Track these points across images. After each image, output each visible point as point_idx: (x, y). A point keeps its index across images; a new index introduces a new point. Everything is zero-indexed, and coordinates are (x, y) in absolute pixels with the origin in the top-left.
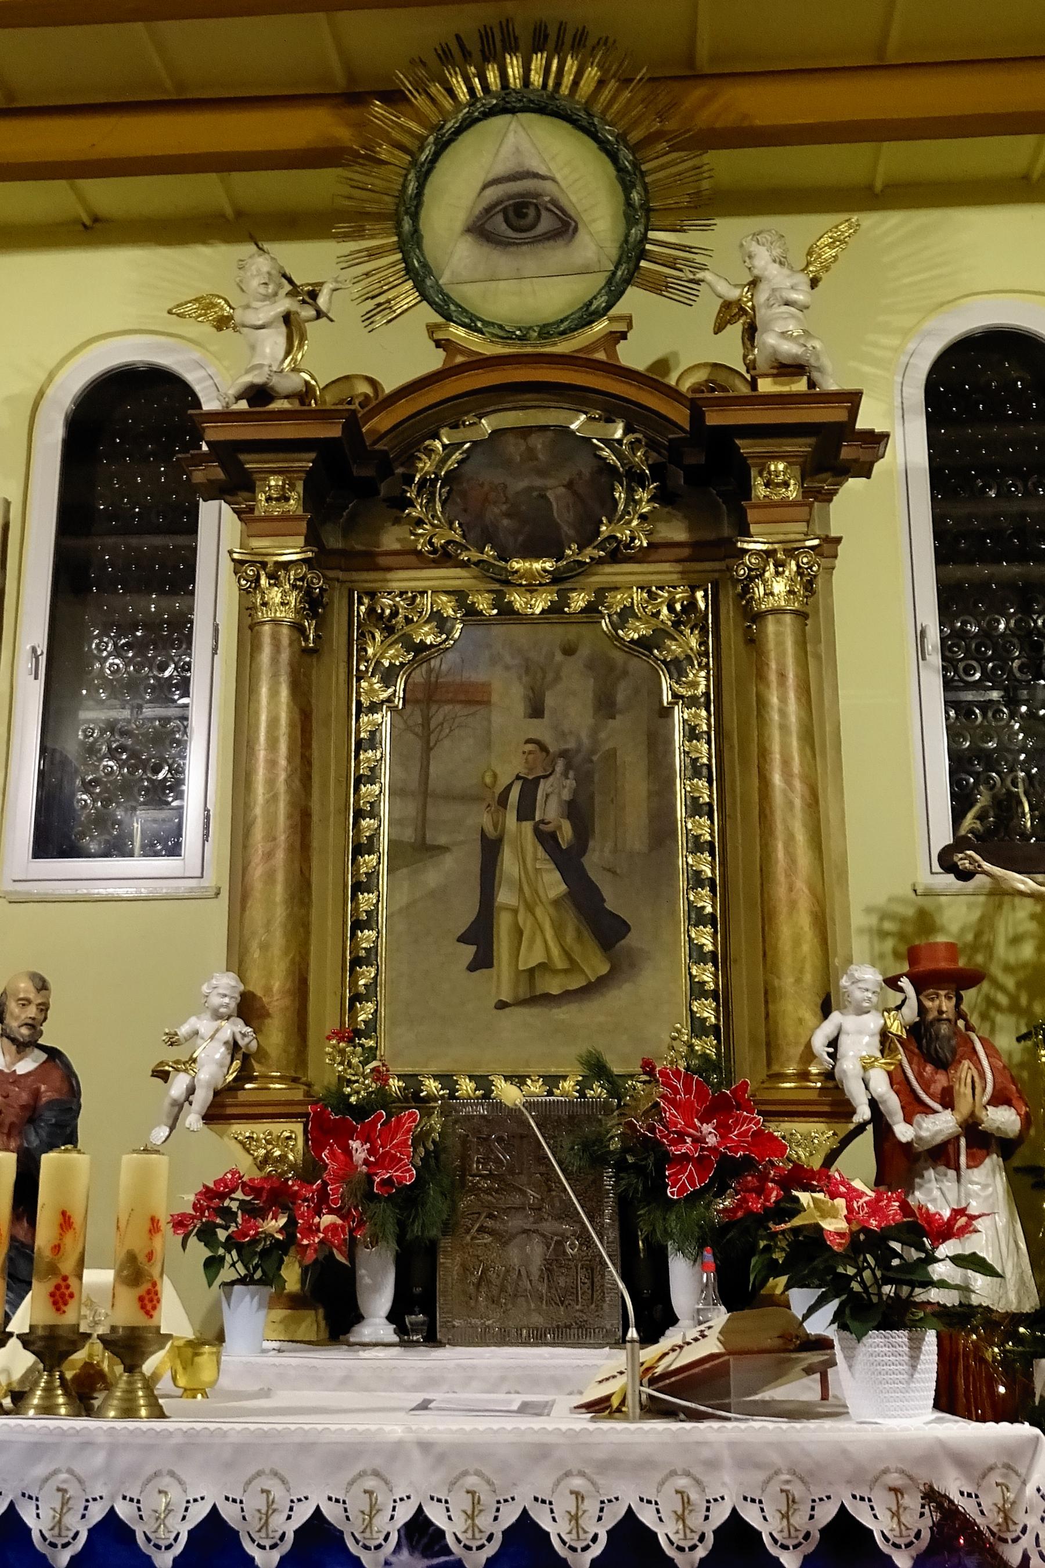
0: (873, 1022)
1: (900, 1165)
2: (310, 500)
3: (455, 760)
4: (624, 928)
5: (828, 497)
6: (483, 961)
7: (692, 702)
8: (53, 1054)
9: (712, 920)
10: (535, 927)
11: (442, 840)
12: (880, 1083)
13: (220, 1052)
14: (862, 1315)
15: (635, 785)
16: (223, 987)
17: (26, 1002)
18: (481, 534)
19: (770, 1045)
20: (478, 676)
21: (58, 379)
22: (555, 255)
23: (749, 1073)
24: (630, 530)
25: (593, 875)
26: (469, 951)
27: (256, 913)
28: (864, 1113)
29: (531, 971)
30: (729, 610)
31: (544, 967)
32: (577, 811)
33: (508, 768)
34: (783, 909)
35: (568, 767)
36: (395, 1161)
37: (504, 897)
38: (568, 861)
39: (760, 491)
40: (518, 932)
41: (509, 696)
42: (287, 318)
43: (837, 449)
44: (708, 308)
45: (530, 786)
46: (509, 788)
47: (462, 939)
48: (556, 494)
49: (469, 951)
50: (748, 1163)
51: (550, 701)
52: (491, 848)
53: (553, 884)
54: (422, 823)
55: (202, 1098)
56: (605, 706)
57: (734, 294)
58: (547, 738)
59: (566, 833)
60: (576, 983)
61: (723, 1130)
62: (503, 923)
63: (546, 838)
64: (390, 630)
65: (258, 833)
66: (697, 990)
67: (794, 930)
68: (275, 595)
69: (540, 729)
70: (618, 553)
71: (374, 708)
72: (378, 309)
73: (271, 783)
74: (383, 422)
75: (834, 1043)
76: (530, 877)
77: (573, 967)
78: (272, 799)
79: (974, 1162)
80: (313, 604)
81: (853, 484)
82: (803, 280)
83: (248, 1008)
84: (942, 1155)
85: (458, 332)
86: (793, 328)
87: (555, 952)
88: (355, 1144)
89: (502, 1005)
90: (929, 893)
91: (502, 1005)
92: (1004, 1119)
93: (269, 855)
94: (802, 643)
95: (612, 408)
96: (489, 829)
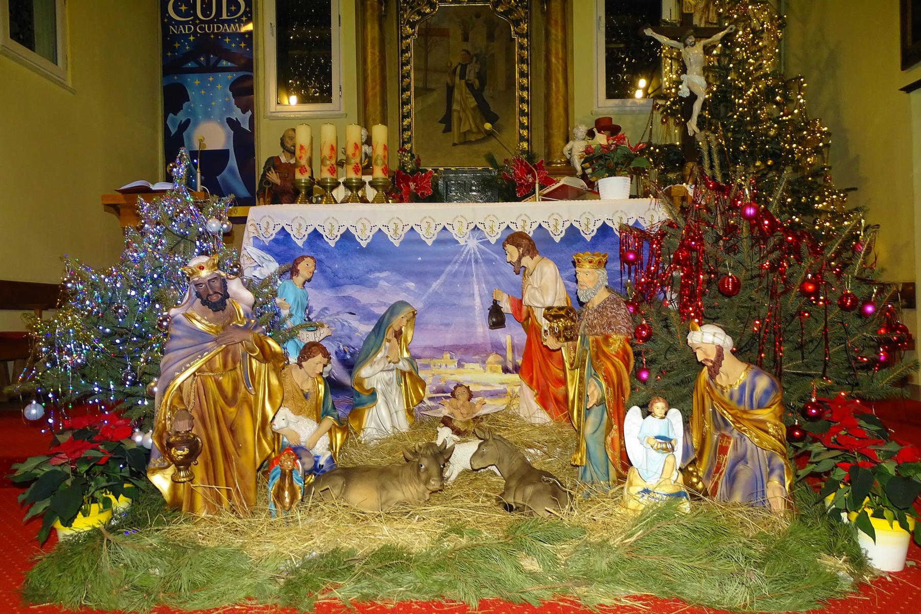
4: (498, 118)
6: (448, 129)
9: (527, 114)
10: (466, 122)
11: (433, 87)
15: (501, 66)
25: (486, 99)
27: (370, 108)
29: (465, 133)
31: (469, 131)
32: (481, 76)
33: (456, 60)
34: (554, 106)
35: (477, 60)
36: (425, 188)
37: (455, 107)
38: (478, 94)
40: (460, 119)
41: (456, 33)
45: (464, 67)
46: (456, 68)
47: (440, 122)
51: (471, 36)
52: (450, 90)
53: (472, 102)
54: (425, 80)
56: (491, 37)
58: (470, 49)
59: (477, 84)
60: (480, 137)
62: (455, 116)
63: (470, 86)
65: (370, 79)
67: (557, 112)
69: (468, 46)
73: (373, 61)
75: (571, 150)
76: (464, 100)
78: (374, 68)
87: (473, 126)
88: (411, 183)
89: (455, 145)
91: (455, 145)
93: (374, 88)
96: (450, 82)
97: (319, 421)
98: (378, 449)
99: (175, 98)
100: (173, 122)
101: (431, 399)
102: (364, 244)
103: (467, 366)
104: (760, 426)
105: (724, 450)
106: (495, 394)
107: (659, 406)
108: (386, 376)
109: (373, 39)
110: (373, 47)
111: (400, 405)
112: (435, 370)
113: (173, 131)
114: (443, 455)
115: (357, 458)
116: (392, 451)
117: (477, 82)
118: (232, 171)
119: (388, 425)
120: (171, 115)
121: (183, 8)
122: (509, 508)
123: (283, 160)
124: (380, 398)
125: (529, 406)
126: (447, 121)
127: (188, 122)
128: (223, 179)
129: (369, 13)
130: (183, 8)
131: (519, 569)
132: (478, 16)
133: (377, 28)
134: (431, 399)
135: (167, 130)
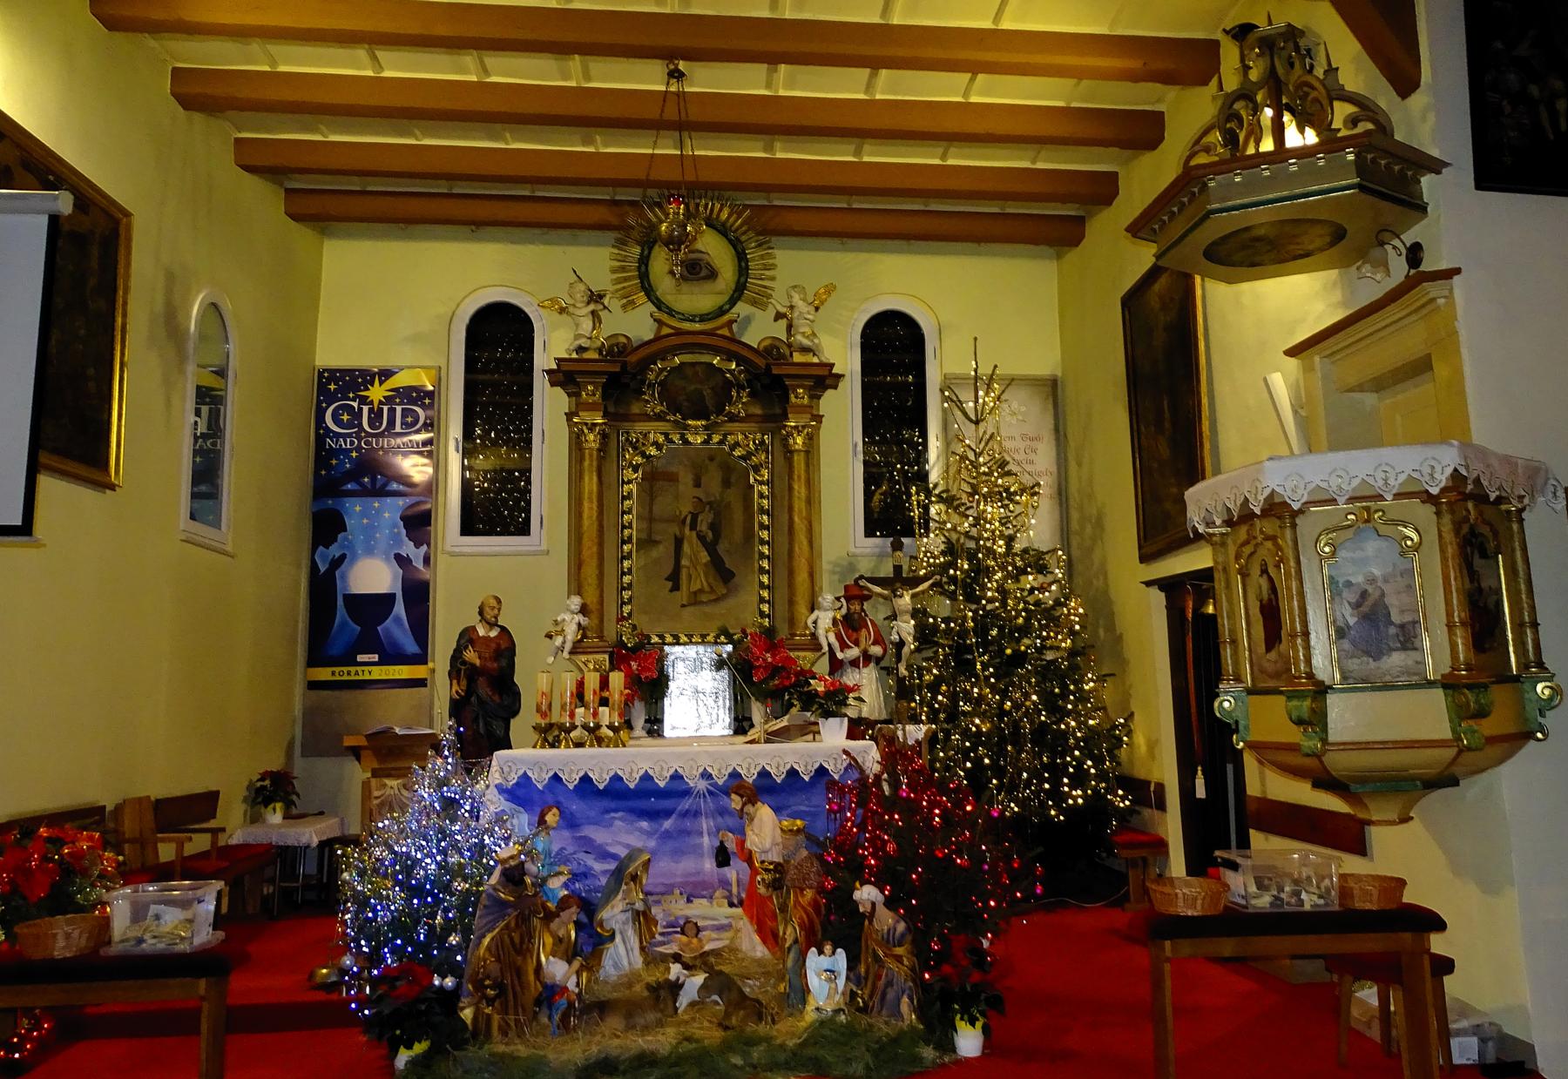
0: (830, 614)
1: (836, 666)
2: (604, 397)
3: (663, 505)
4: (732, 575)
5: (819, 397)
6: (676, 587)
7: (761, 483)
8: (503, 629)
10: (697, 578)
11: (658, 538)
12: (832, 638)
13: (574, 627)
14: (827, 714)
15: (738, 515)
16: (576, 602)
17: (493, 608)
18: (674, 407)
19: (792, 622)
20: (673, 469)
21: (462, 306)
22: (708, 286)
23: (783, 633)
24: (738, 409)
26: (670, 584)
28: (826, 648)
30: (777, 444)
31: (701, 591)
32: (714, 527)
33: (686, 509)
37: (684, 562)
39: (793, 399)
41: (686, 479)
42: (593, 313)
43: (825, 379)
44: (771, 313)
45: (695, 517)
47: (667, 579)
48: (707, 392)
49: (670, 584)
50: (783, 668)
51: (704, 480)
52: (679, 542)
53: (704, 557)
55: (568, 646)
56: (726, 483)
57: (783, 310)
58: (702, 496)
61: (773, 656)
62: (684, 573)
63: (701, 538)
64: (635, 448)
66: (762, 600)
67: (802, 577)
68: (591, 437)
69: (699, 493)
70: (733, 418)
71: (630, 482)
72: (629, 305)
74: (633, 359)
75: (815, 622)
77: (712, 591)
79: (866, 665)
80: (604, 436)
81: (830, 392)
82: (812, 309)
83: (584, 610)
84: (854, 663)
85: (665, 318)
86: (808, 331)
90: (855, 556)
92: (876, 650)
94: (807, 465)
95: (729, 356)
97: (569, 962)
98: (616, 987)
99: (327, 527)
100: (323, 557)
101: (662, 934)
102: (601, 787)
103: (696, 901)
104: (899, 959)
105: (879, 977)
106: (720, 928)
107: (828, 948)
108: (623, 917)
109: (590, 493)
110: (591, 501)
111: (634, 942)
112: (665, 906)
113: (322, 569)
114: (676, 987)
115: (605, 994)
116: (630, 985)
117: (710, 534)
118: (398, 620)
119: (625, 963)
120: (321, 548)
121: (345, 417)
122: (726, 1028)
123: (481, 632)
124: (618, 938)
125: (751, 939)
126: (674, 579)
127: (343, 557)
128: (387, 630)
129: (586, 463)
130: (345, 417)
131: (727, 1061)
132: (712, 459)
133: (595, 478)
134: (662, 934)
135: (314, 566)
